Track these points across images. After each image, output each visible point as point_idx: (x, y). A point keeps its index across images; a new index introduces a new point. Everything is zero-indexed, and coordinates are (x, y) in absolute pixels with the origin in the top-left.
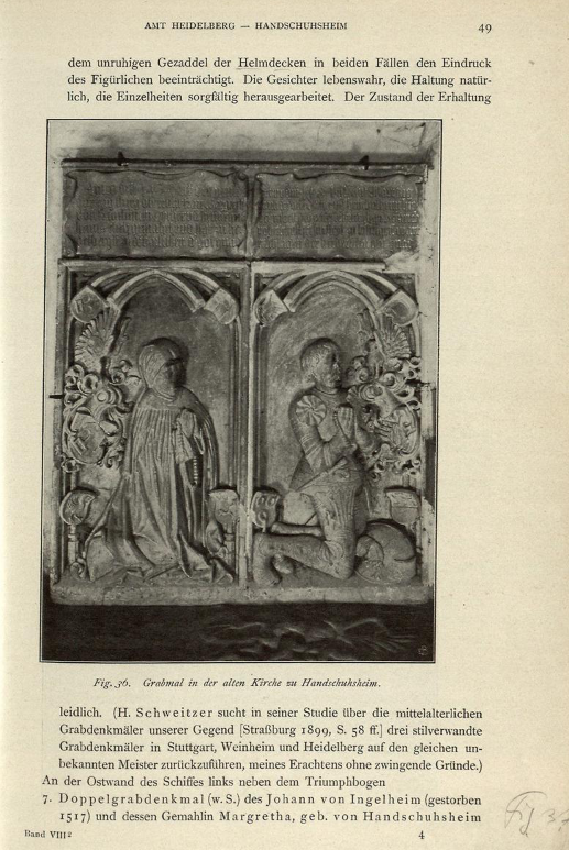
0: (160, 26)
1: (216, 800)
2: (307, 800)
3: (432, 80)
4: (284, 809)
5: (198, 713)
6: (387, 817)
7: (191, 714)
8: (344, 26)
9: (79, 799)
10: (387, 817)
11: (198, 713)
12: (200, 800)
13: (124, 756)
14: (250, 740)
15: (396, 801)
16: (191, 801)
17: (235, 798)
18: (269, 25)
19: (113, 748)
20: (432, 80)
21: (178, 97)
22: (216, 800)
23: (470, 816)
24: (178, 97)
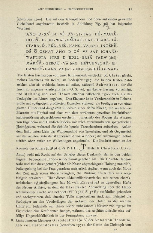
0: (42, 9)
1: (81, 220)
2: (100, 220)
3: (22, 169)
4: (56, 223)
5: (113, 85)
6: (44, 225)
7: (111, 85)
8: (92, 9)
9: (64, 221)
10: (44, 225)
11: (113, 85)
12: (77, 220)
13: (124, 166)
14: (88, 116)
15: (84, 187)
16: (74, 221)
17: (86, 220)
18: (75, 45)
19: (95, 155)
20: (22, 169)
21: (34, 141)
22: (81, 220)
23: (127, 219)
24: (34, 141)
